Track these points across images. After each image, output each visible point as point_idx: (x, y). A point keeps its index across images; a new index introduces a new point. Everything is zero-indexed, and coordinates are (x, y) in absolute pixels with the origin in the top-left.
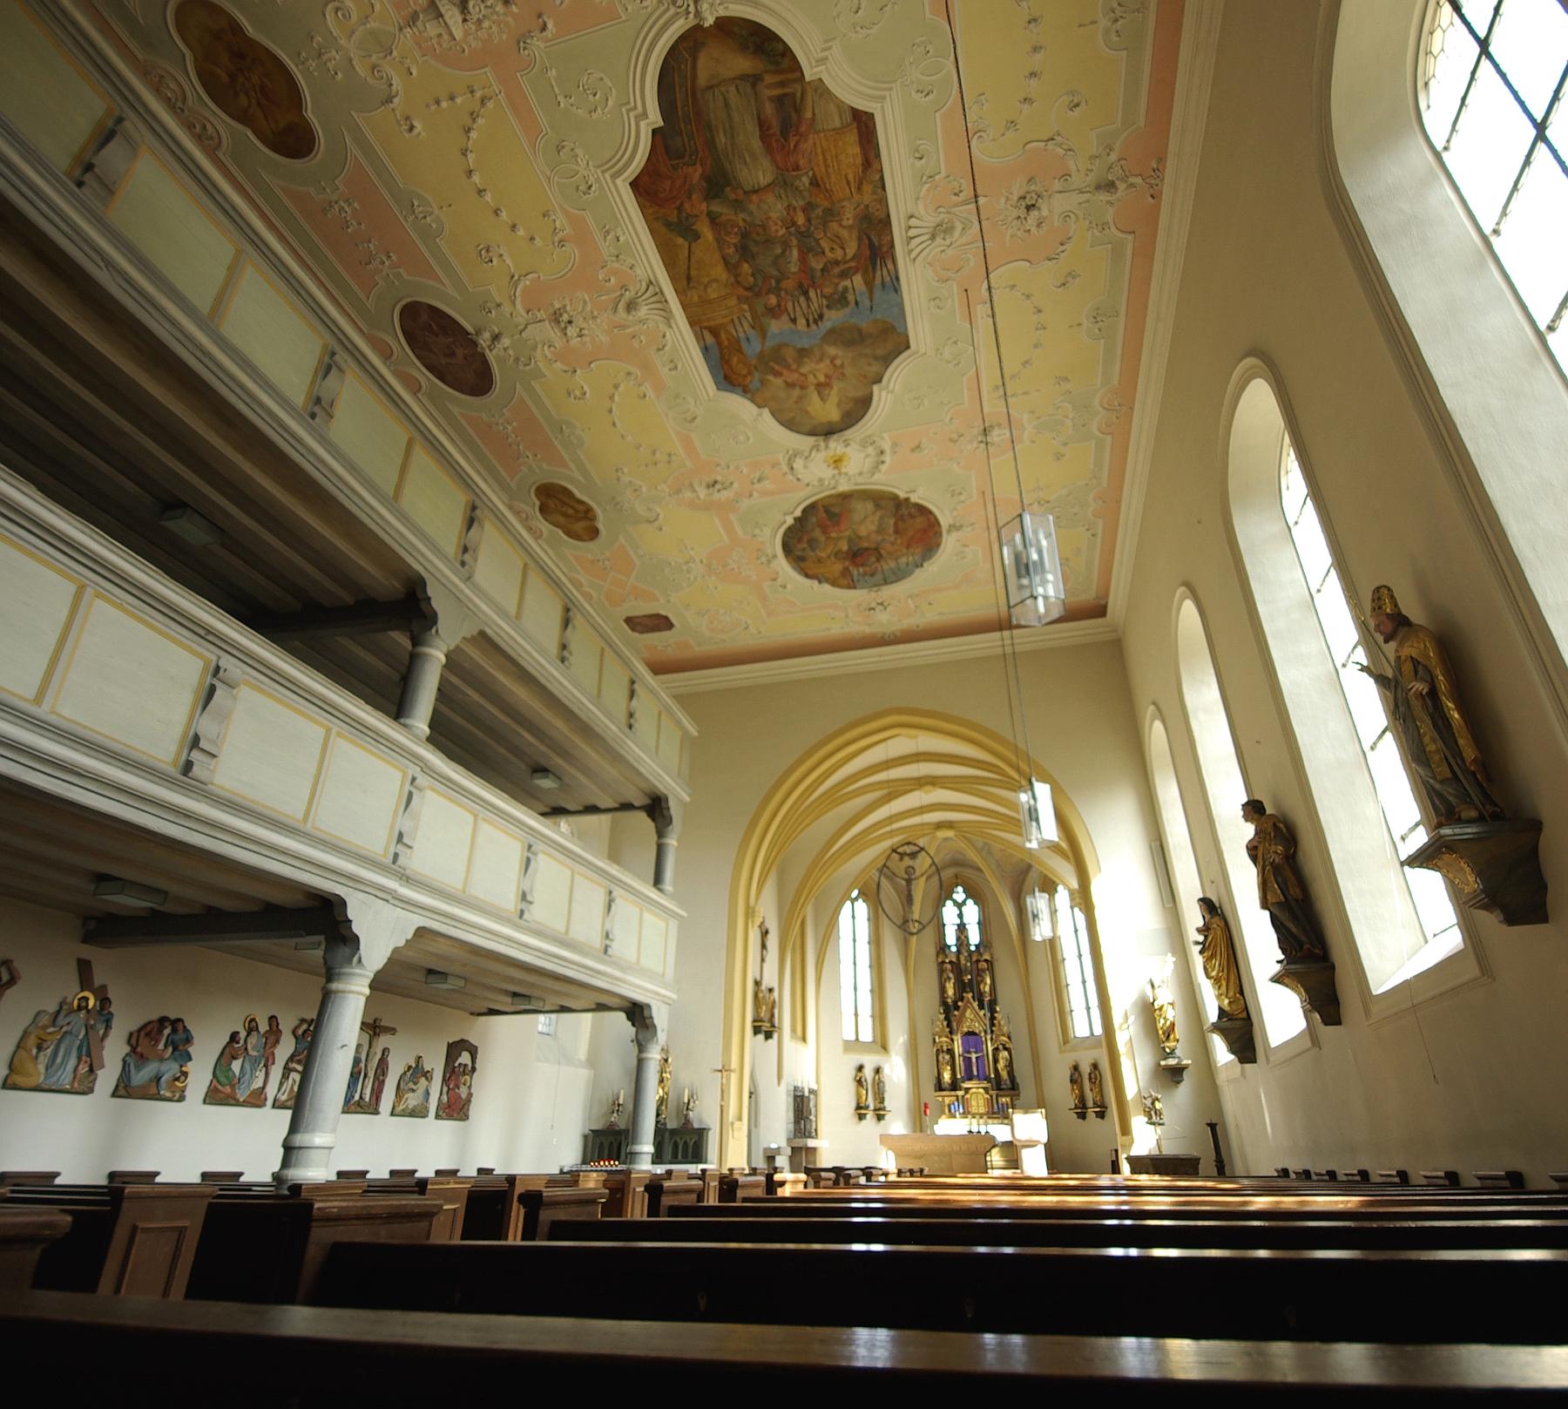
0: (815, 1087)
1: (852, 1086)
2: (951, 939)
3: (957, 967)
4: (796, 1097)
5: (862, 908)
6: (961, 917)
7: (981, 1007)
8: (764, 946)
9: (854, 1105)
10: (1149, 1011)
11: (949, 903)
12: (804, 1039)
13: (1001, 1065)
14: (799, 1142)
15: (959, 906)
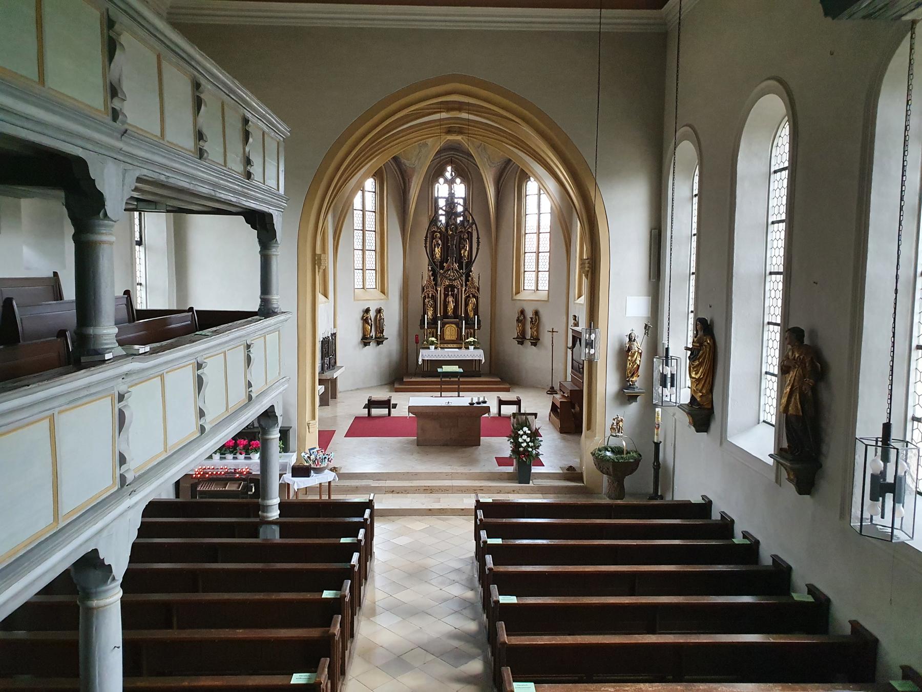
1: (360, 323)
7: (461, 267)
9: (361, 336)
10: (625, 353)
11: (441, 180)
12: (326, 296)
13: (470, 307)
15: (451, 182)
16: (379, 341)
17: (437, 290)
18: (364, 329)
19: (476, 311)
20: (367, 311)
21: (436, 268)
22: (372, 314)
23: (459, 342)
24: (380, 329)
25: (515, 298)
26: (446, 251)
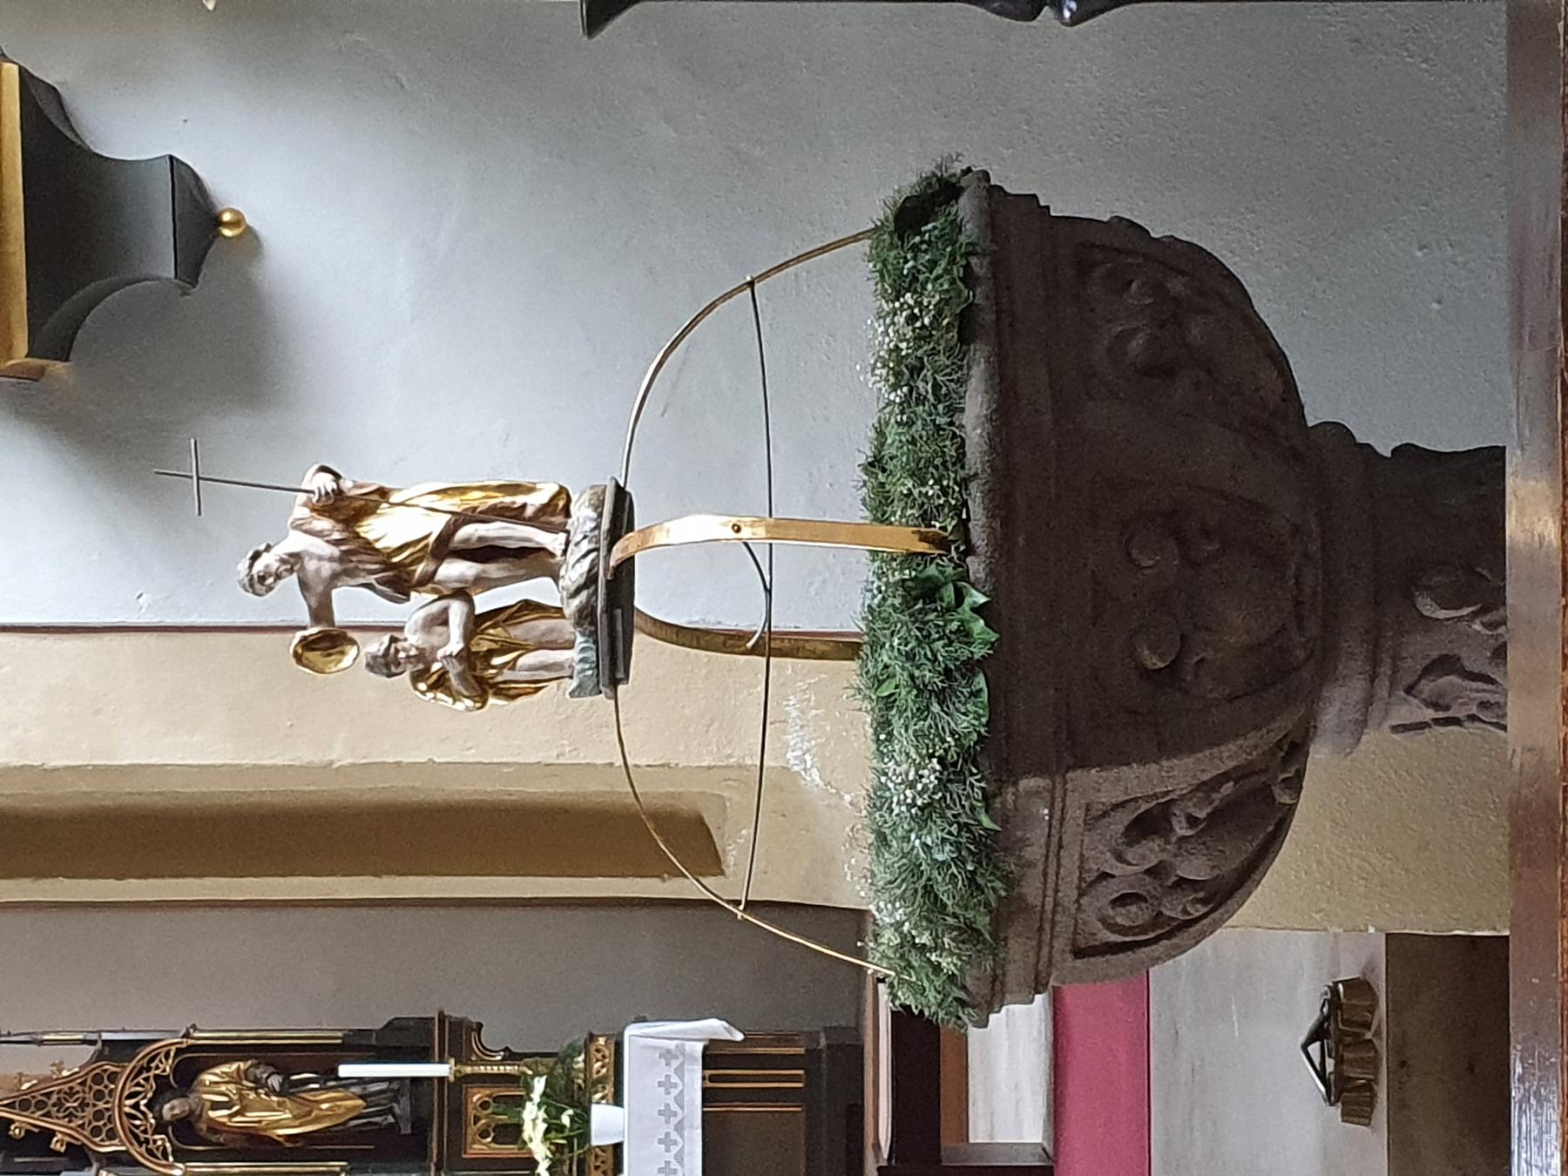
13: (280, 1120)
19: (293, 1062)
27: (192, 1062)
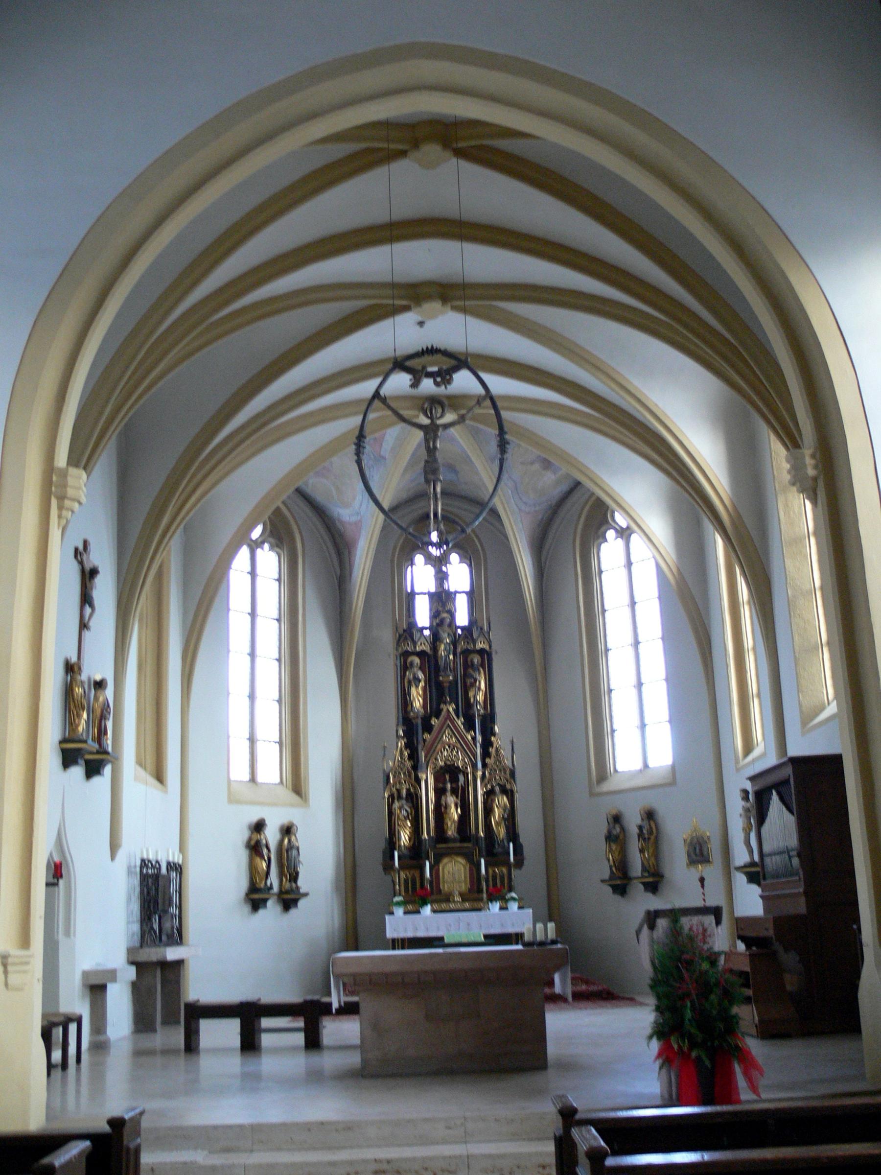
0: (177, 858)
1: (243, 855)
2: (423, 616)
3: (430, 661)
4: (144, 878)
5: (269, 561)
6: (438, 582)
7: (470, 726)
8: (86, 599)
9: (243, 885)
12: (159, 776)
14: (152, 954)
15: (439, 563)
16: (289, 900)
17: (418, 781)
18: (252, 870)
20: (259, 827)
21: (413, 729)
22: (271, 836)
23: (476, 896)
24: (290, 873)
25: (598, 790)
26: (437, 693)
27: (510, 794)
